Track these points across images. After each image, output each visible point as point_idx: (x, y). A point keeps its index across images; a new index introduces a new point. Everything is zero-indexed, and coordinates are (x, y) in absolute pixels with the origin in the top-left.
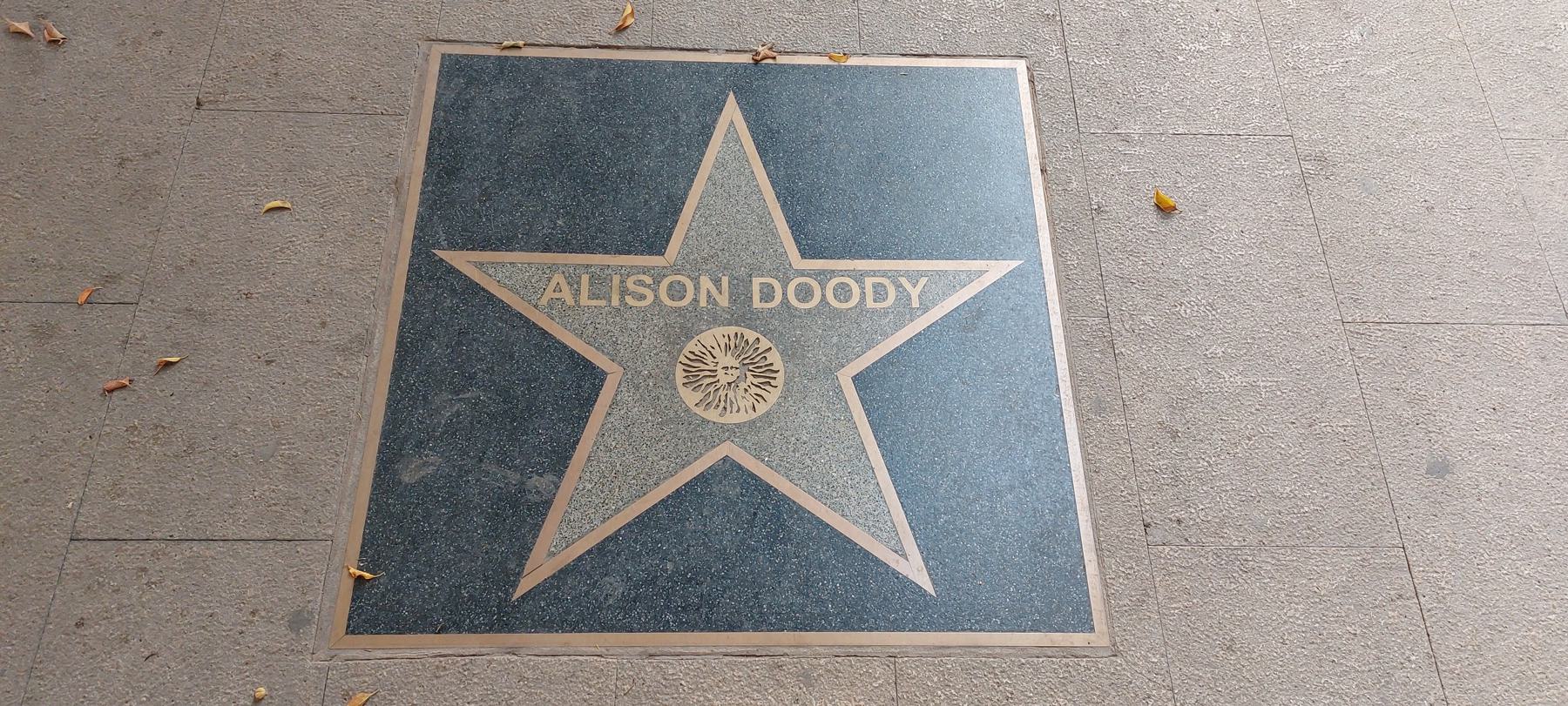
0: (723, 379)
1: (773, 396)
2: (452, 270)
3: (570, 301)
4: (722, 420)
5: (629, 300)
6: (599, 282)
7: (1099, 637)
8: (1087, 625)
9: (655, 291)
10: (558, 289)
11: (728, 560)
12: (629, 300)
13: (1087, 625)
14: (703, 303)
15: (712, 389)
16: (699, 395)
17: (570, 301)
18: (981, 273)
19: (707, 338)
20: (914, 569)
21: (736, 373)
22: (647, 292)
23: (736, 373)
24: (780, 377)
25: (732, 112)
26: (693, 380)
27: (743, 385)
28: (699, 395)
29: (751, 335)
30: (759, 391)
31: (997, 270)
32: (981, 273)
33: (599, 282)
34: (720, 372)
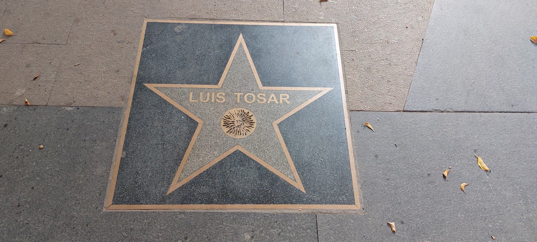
0: (236, 124)
1: (252, 130)
2: (304, 184)
3: (277, 102)
4: (235, 137)
5: (217, 100)
6: (277, 94)
7: (357, 206)
8: (352, 202)
9: (257, 98)
10: (273, 98)
11: (237, 182)
12: (217, 100)
13: (352, 202)
14: (213, 101)
15: (232, 127)
16: (228, 129)
17: (277, 102)
18: (320, 92)
19: (232, 111)
20: (299, 185)
21: (241, 123)
22: (223, 98)
23: (241, 123)
24: (255, 125)
25: (241, 39)
26: (226, 124)
27: (242, 127)
28: (228, 129)
29: (246, 111)
30: (247, 129)
31: (325, 90)
32: (320, 92)
33: (277, 94)
34: (235, 123)
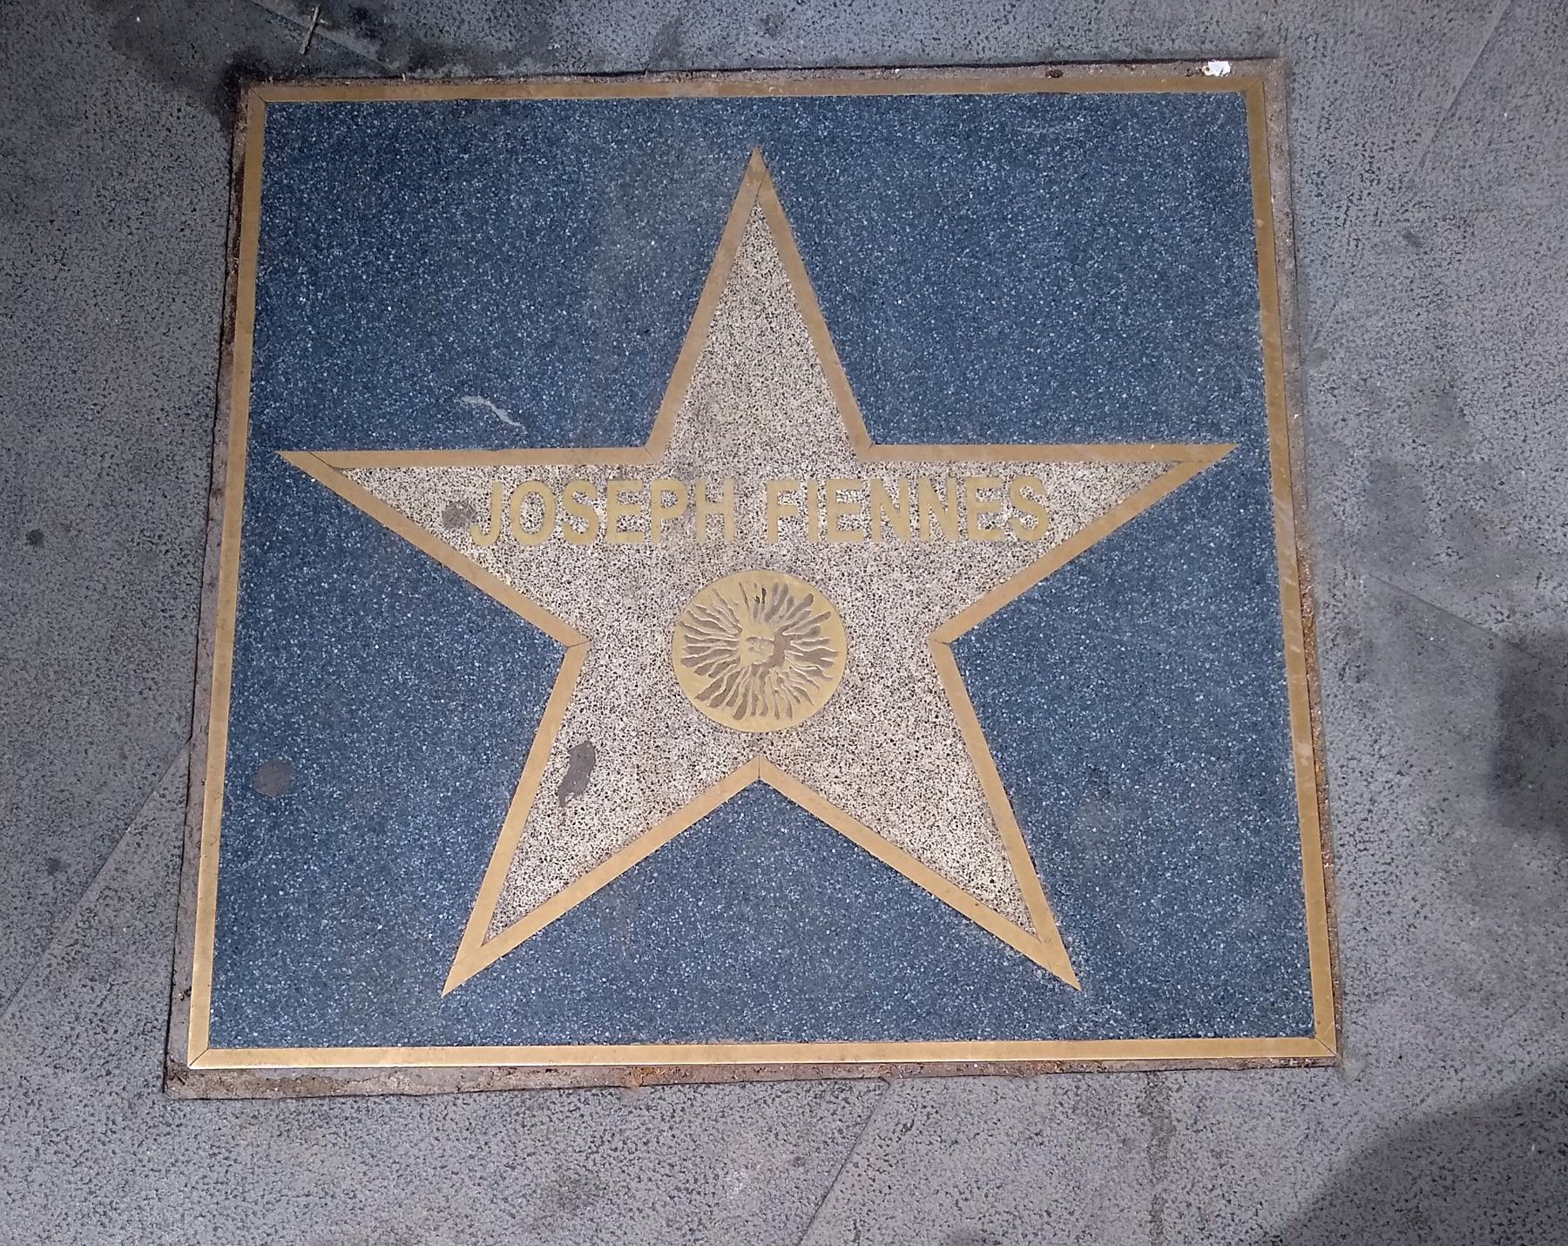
15: (725, 675)
